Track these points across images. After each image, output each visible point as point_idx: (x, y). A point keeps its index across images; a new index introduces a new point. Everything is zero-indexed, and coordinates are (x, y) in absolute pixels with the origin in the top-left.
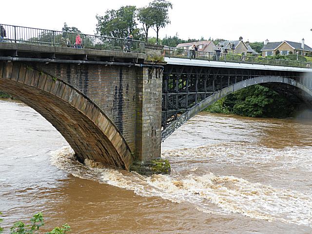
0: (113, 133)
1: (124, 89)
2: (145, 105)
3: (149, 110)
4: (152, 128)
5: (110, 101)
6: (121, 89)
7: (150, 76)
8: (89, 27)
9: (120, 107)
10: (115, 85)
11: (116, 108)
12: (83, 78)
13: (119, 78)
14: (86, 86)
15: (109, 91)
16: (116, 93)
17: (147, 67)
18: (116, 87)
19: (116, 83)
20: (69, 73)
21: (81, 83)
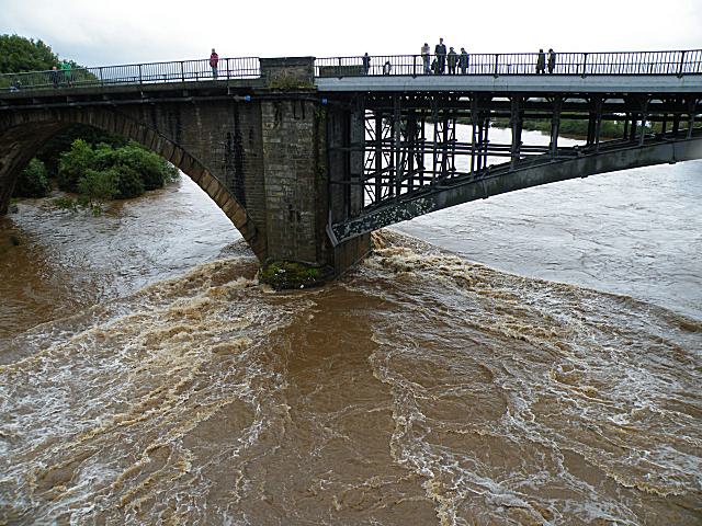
0: (228, 203)
1: (245, 138)
2: (270, 166)
3: (280, 174)
4: (291, 207)
5: (220, 154)
6: (238, 136)
7: (279, 116)
8: (60, 59)
9: (239, 166)
10: (227, 131)
11: (230, 166)
12: (174, 121)
13: (233, 119)
14: (179, 132)
15: (216, 140)
16: (229, 143)
17: (269, 100)
18: (229, 134)
19: (227, 127)
20: (141, 112)
21: (171, 128)
